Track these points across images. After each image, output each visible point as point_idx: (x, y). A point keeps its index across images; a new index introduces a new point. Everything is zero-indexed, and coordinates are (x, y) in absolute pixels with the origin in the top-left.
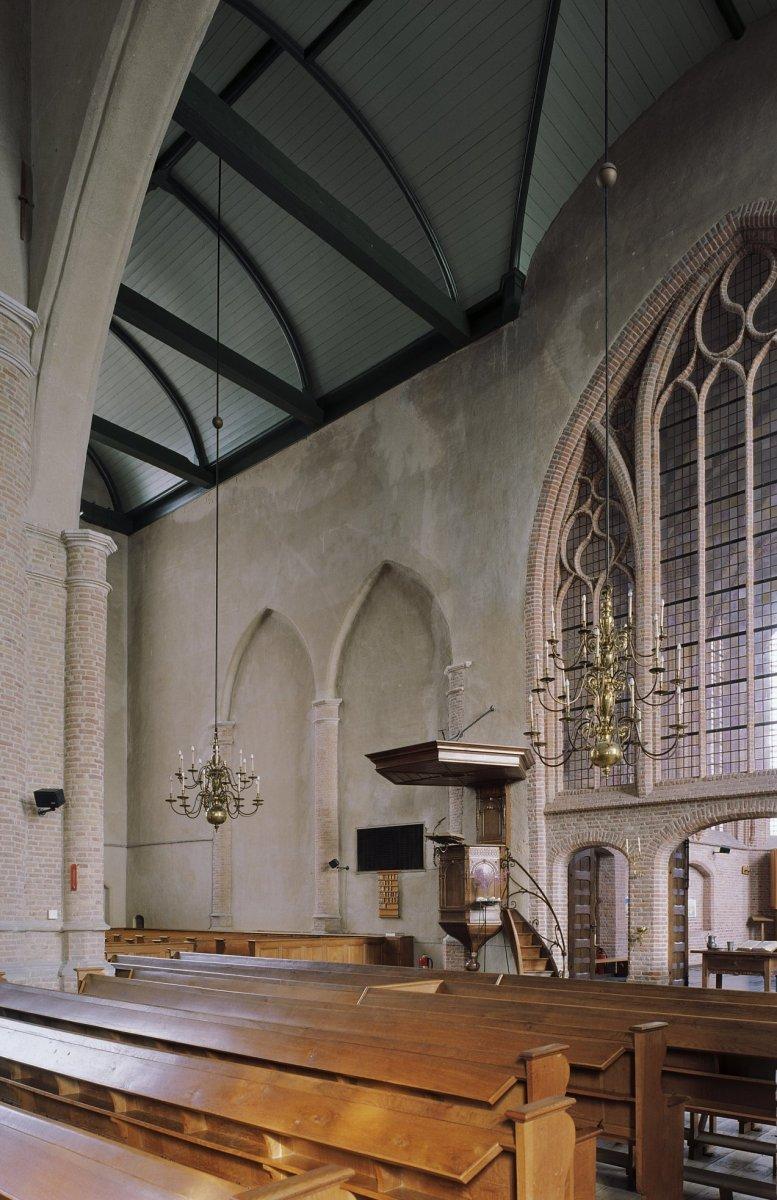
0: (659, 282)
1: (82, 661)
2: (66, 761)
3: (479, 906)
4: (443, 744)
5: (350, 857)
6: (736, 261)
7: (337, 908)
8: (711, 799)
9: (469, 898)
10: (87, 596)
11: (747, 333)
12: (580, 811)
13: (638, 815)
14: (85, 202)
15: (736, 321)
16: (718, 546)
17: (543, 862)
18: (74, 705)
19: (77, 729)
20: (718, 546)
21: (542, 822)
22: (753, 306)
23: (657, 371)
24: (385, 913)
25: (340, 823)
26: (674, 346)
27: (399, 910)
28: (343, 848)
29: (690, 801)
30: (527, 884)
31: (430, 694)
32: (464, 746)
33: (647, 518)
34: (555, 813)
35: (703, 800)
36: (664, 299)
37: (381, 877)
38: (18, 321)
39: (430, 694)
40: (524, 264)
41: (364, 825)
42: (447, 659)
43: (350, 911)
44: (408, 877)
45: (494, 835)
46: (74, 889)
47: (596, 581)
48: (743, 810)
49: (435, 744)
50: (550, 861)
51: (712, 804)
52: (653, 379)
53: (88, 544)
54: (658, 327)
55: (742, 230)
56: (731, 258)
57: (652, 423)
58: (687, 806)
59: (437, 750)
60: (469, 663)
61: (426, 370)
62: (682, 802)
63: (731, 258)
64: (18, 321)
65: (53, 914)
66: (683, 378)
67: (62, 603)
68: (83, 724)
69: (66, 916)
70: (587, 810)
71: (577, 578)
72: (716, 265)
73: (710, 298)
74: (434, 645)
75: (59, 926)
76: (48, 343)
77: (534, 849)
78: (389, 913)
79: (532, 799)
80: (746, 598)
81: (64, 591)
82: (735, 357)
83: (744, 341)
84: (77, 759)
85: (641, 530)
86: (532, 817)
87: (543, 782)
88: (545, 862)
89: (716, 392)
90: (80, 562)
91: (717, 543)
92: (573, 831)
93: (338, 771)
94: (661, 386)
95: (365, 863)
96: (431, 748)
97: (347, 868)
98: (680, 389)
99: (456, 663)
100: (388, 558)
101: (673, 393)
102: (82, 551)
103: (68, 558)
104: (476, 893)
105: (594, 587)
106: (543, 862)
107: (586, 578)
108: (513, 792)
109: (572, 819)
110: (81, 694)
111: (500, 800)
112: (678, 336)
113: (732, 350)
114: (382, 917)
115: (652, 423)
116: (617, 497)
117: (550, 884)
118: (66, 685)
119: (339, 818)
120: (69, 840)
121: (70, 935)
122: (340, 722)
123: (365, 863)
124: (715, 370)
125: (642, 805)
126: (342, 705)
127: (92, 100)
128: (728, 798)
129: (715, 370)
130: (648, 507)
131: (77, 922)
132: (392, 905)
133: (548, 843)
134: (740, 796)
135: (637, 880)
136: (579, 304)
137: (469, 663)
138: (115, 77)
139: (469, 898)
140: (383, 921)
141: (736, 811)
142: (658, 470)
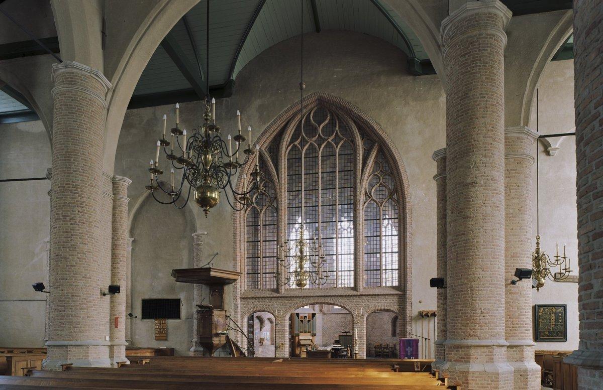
0: (289, 106)
1: (121, 231)
2: (113, 273)
3: (217, 335)
4: (213, 269)
5: (138, 312)
6: (316, 108)
7: (130, 336)
8: (307, 296)
9: (214, 332)
10: (123, 204)
11: (319, 135)
12: (256, 298)
13: (279, 301)
14: (139, 47)
15: (316, 129)
16: (308, 207)
17: (239, 317)
18: (117, 249)
19: (119, 260)
20: (308, 207)
21: (239, 300)
22: (321, 126)
23: (287, 138)
24: (158, 338)
25: (131, 296)
26: (293, 130)
27: (166, 336)
28: (134, 307)
29: (300, 297)
30: (232, 325)
31: (184, 243)
32: (218, 270)
33: (283, 191)
34: (245, 298)
35: (304, 297)
36: (291, 112)
37: (156, 322)
38: (104, 85)
39: (184, 243)
40: (234, 77)
41: (146, 297)
42: (193, 229)
43: (137, 337)
44: (171, 323)
45: (220, 306)
46: (116, 327)
47: (262, 210)
48: (318, 301)
49: (210, 268)
50: (242, 317)
51: (307, 298)
52: (286, 140)
53: (123, 183)
54: (288, 122)
55: (318, 99)
56: (314, 107)
57: (285, 156)
58: (298, 299)
59: (210, 271)
60: (206, 233)
61: (185, 104)
62: (297, 297)
63: (314, 107)
64: (104, 85)
65: (108, 338)
66: (296, 143)
67: (111, 205)
68: (121, 258)
69: (111, 339)
70: (258, 298)
71: (254, 207)
72: (310, 107)
73: (306, 118)
74: (186, 222)
75: (109, 344)
76: (114, 98)
77: (236, 312)
78: (161, 338)
79: (235, 292)
80: (319, 227)
81: (112, 201)
82: (315, 141)
83: (318, 137)
84: (118, 273)
85: (281, 195)
86: (235, 299)
87: (239, 285)
88: (240, 317)
89: (308, 152)
90: (120, 190)
91: (308, 205)
92: (252, 305)
93: (131, 272)
94: (288, 143)
95: (146, 315)
96: (209, 270)
97: (136, 317)
98: (295, 146)
99: (199, 232)
100: (163, 180)
101: (292, 147)
102: (121, 185)
103: (113, 187)
104: (216, 329)
105: (261, 212)
106: (239, 317)
107: (258, 208)
108: (228, 289)
109: (252, 301)
110: (120, 245)
111: (221, 293)
112: (295, 127)
113: (314, 139)
114: (156, 340)
115: (285, 156)
116: (272, 181)
117: (242, 326)
118: (112, 240)
119: (131, 293)
120: (114, 306)
121: (115, 347)
122: (132, 249)
123: (146, 315)
124: (308, 144)
125: (281, 297)
126: (134, 242)
127: (150, 14)
128: (313, 297)
129: (308, 144)
130: (283, 187)
131: (117, 341)
132: (162, 335)
133: (241, 309)
134: (317, 296)
135: (279, 325)
136: (257, 102)
137: (206, 233)
138: (162, 10)
139: (214, 332)
140: (157, 342)
141: (316, 301)
142: (286, 174)
